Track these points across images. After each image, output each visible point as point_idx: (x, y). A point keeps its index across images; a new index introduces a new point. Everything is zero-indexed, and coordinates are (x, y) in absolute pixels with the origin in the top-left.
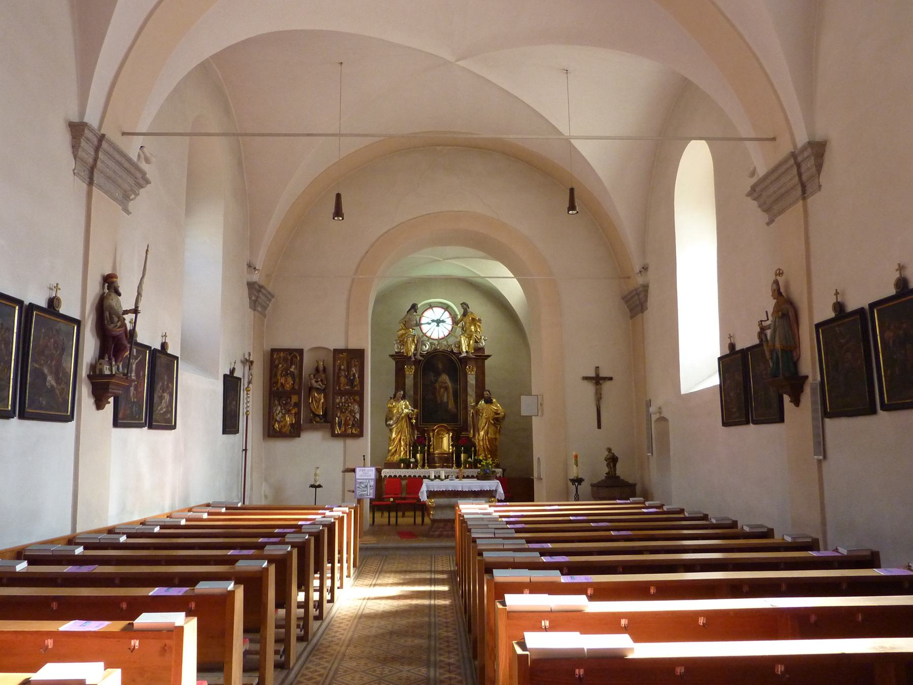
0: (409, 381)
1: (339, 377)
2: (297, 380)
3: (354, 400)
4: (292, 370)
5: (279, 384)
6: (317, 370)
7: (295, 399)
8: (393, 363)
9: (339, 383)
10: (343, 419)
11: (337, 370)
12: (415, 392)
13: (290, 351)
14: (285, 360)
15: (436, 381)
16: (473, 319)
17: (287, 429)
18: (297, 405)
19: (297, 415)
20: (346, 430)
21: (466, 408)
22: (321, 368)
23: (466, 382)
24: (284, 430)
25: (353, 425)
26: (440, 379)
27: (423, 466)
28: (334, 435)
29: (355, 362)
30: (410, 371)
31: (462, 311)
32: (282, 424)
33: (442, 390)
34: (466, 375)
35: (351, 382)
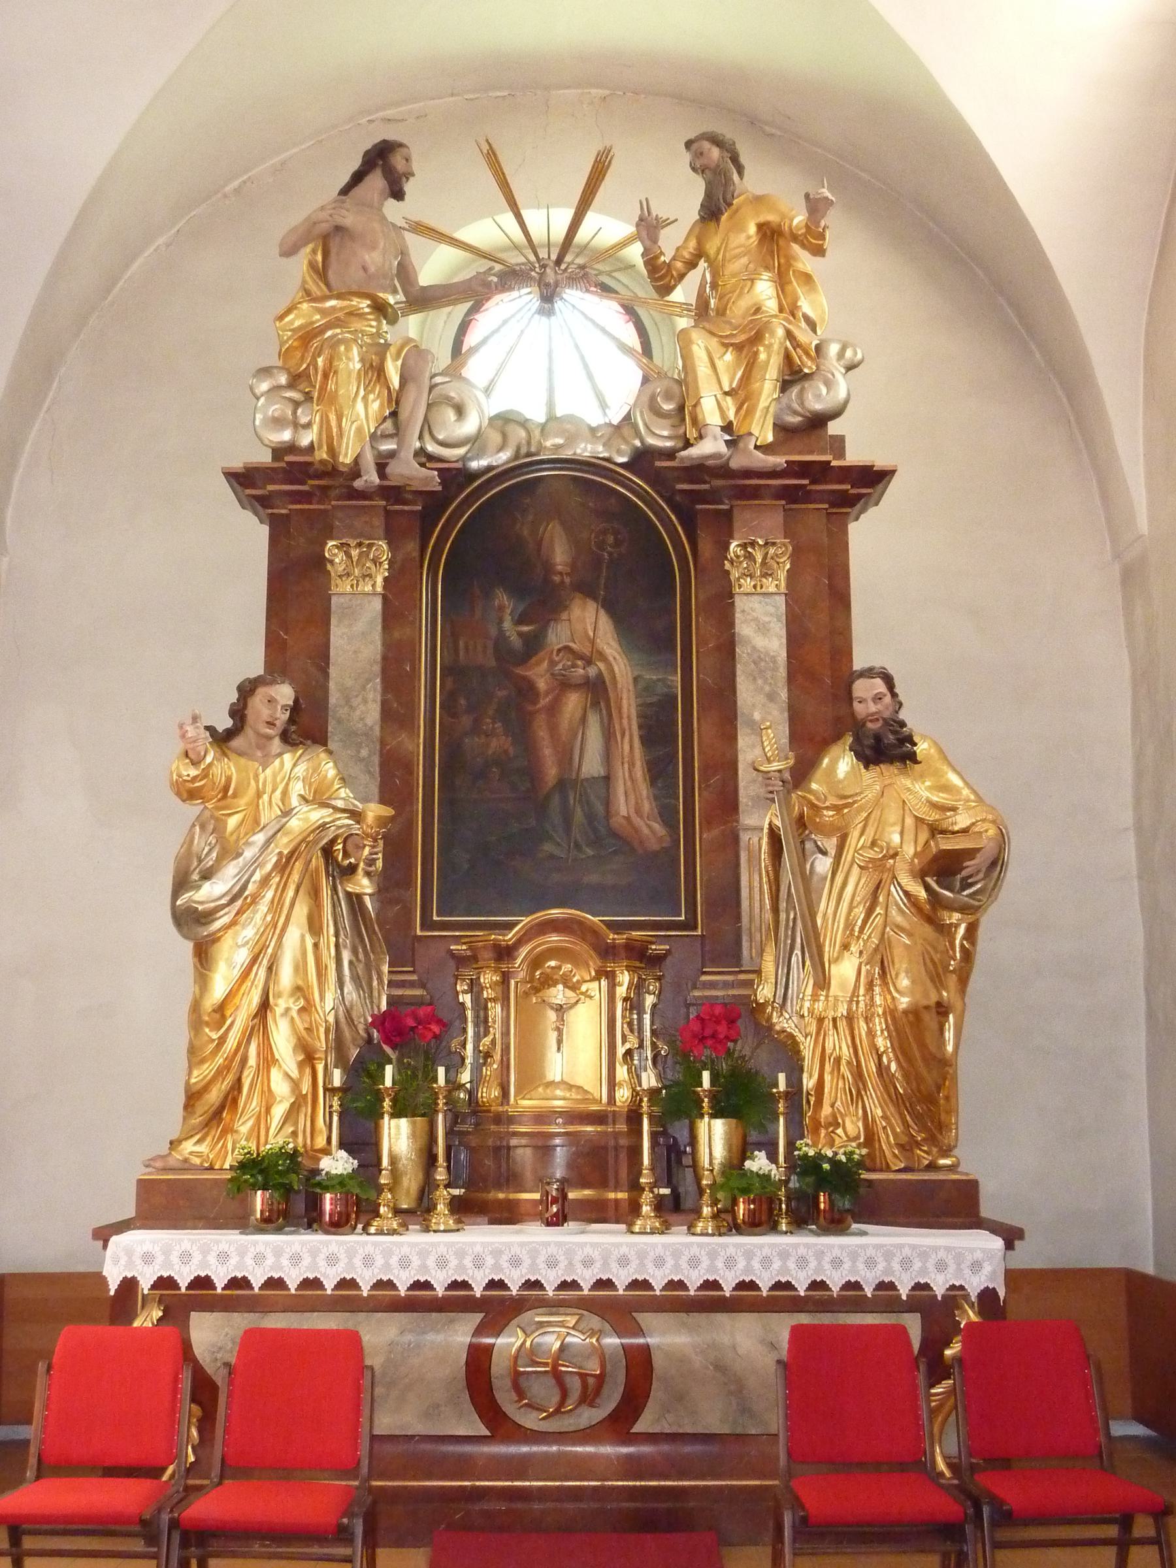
0: (355, 636)
8: (251, 536)
12: (395, 714)
15: (533, 645)
16: (770, 234)
21: (727, 804)
23: (727, 648)
26: (558, 635)
27: (419, 1213)
30: (358, 579)
31: (695, 191)
33: (573, 702)
34: (722, 605)
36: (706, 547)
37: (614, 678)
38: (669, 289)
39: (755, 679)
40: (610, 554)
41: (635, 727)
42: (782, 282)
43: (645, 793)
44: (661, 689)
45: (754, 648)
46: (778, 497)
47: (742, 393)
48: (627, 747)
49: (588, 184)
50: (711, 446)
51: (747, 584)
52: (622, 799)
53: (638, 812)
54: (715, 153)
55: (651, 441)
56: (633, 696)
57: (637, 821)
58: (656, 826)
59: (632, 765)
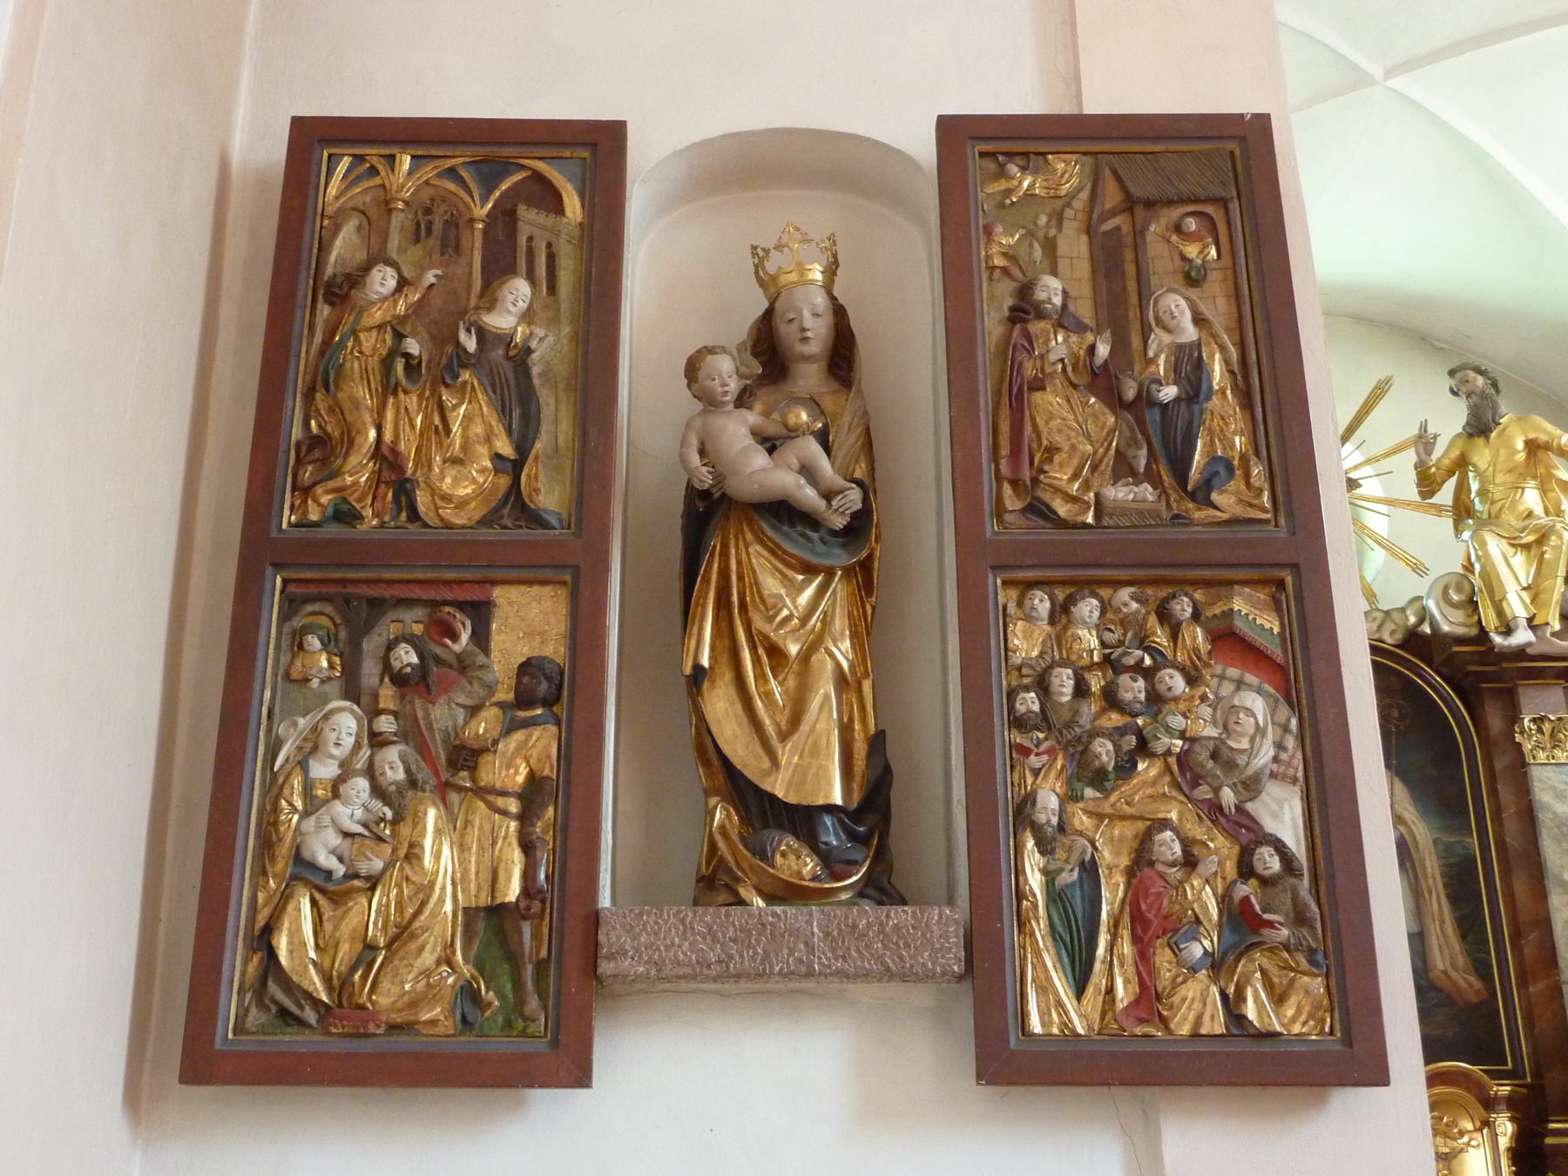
1: (1017, 394)
2: (557, 424)
3: (1228, 639)
4: (502, 320)
5: (358, 471)
6: (769, 351)
7: (526, 623)
9: (1023, 456)
10: (1112, 858)
11: (992, 323)
13: (489, 146)
14: (437, 228)
17: (425, 978)
18: (547, 690)
19: (557, 808)
20: (1150, 1000)
22: (817, 330)
24: (388, 994)
25: (1242, 923)
28: (1009, 1062)
29: (1169, 243)
32: (370, 914)
35: (1162, 438)
36: (1495, 722)
37: (1417, 844)
38: (1432, 494)
39: (1560, 843)
40: (1397, 727)
41: (1440, 886)
42: (1544, 491)
43: (1458, 948)
44: (1459, 850)
45: (1555, 813)
46: (1558, 677)
47: (1534, 591)
48: (1435, 907)
49: (1367, 402)
50: (1522, 636)
51: (1542, 756)
52: (1437, 952)
53: (1454, 965)
54: (1480, 381)
55: (1446, 628)
56: (1434, 857)
57: (1454, 974)
58: (1473, 980)
59: (1442, 922)
